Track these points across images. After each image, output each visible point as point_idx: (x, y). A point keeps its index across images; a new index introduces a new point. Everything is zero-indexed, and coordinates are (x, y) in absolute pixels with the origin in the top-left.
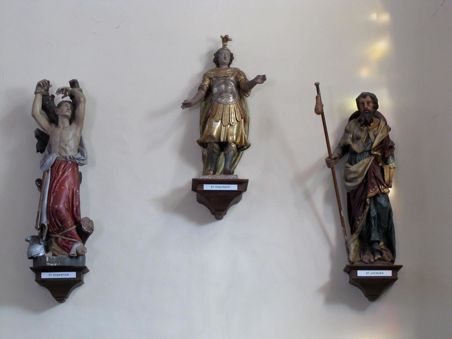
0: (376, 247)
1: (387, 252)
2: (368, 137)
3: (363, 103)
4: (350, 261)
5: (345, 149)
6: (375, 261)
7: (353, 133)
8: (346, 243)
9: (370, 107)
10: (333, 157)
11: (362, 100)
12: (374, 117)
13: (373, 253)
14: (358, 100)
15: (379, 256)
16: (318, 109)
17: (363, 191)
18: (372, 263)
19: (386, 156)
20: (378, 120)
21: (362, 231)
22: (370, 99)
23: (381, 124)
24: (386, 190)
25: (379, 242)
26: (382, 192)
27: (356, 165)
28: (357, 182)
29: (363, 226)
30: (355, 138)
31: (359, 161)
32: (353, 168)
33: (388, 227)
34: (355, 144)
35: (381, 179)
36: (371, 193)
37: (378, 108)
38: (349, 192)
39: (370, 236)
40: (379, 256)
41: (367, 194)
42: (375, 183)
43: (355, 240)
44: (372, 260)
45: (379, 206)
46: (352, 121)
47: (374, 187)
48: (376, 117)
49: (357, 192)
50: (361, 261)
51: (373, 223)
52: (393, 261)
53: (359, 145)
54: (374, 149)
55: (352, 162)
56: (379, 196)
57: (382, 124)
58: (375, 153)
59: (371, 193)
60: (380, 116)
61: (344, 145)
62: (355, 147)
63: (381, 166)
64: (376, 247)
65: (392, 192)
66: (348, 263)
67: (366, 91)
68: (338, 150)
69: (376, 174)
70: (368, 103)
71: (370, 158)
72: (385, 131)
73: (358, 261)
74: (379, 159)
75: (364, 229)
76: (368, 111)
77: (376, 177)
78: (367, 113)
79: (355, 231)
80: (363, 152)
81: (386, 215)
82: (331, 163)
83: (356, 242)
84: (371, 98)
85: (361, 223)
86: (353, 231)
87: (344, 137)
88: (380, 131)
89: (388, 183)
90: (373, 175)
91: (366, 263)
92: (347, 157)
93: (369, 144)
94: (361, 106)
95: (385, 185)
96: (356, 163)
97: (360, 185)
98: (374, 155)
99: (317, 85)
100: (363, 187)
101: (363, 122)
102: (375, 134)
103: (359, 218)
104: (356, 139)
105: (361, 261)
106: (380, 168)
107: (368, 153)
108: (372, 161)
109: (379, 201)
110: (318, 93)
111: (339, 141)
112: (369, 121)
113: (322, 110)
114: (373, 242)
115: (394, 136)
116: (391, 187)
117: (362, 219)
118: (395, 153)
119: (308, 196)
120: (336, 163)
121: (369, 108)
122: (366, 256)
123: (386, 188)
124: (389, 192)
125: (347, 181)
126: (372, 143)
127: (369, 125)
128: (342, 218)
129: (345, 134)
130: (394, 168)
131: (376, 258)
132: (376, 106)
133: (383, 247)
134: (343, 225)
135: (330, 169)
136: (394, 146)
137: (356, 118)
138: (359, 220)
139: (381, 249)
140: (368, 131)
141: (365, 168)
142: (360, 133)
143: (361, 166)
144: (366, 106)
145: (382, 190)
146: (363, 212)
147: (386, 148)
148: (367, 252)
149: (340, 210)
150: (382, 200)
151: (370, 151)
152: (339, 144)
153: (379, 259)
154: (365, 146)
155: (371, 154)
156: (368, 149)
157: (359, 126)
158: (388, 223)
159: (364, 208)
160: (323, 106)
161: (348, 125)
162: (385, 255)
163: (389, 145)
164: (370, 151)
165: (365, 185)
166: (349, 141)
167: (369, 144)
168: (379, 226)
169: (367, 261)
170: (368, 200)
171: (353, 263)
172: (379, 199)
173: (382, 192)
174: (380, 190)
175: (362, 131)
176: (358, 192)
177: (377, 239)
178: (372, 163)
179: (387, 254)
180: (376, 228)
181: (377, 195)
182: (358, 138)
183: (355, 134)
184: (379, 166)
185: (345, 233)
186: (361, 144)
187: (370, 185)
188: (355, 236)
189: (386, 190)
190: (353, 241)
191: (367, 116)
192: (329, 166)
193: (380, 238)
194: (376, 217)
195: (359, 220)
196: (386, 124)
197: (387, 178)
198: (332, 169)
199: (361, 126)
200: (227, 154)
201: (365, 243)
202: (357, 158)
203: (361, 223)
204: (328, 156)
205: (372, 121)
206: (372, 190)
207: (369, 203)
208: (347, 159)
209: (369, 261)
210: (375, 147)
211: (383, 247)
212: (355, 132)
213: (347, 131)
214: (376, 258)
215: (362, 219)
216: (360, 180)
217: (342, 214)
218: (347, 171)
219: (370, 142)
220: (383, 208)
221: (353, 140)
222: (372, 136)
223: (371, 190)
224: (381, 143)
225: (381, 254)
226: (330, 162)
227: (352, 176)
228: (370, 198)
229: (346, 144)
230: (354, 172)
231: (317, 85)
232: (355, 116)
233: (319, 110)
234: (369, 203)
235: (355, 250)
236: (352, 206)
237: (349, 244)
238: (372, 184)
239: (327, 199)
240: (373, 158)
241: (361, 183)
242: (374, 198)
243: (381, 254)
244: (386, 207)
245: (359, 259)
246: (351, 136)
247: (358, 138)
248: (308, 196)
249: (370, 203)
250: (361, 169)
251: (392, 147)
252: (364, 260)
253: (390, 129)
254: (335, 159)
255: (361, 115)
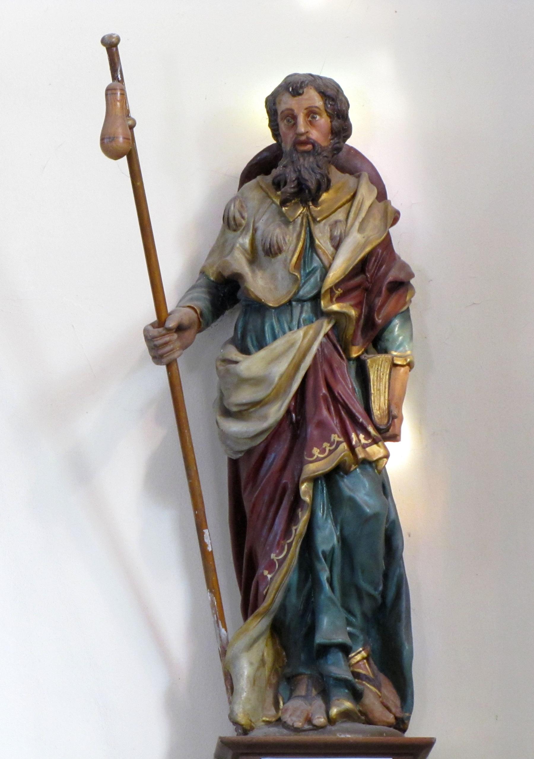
0: (337, 667)
1: (379, 688)
2: (311, 245)
3: (292, 117)
4: (235, 723)
5: (224, 293)
6: (331, 721)
7: (255, 230)
8: (223, 653)
9: (318, 132)
10: (171, 323)
11: (288, 102)
12: (333, 169)
13: (325, 689)
14: (272, 104)
15: (348, 705)
16: (113, 139)
17: (290, 451)
18: (316, 728)
19: (379, 321)
20: (351, 180)
21: (283, 607)
22: (318, 102)
23: (359, 197)
24: (375, 451)
25: (346, 650)
26: (361, 456)
27: (262, 353)
28: (265, 418)
29: (288, 590)
30: (260, 248)
31: (275, 338)
32: (251, 365)
33: (384, 595)
34: (259, 274)
35: (358, 409)
36: (318, 463)
37: (348, 136)
38: (235, 457)
39: (312, 630)
40: (348, 705)
41: (302, 463)
42: (334, 423)
43: (256, 640)
44: (320, 720)
45: (347, 512)
46: (253, 182)
47: (328, 440)
48: (343, 169)
49: (263, 456)
50: (279, 722)
51: (324, 576)
52: (401, 724)
53: (273, 277)
54: (331, 290)
55: (247, 341)
56: (347, 472)
57: (366, 195)
58: (335, 307)
59: (318, 463)
60: (355, 166)
61: (220, 275)
62: (262, 285)
63: (358, 358)
64: (337, 667)
65: (401, 458)
66: (230, 732)
67: (303, 69)
68: (196, 294)
69: (339, 389)
70: (311, 113)
71: (315, 325)
72: (375, 222)
73: (268, 723)
74: (350, 331)
75: (293, 599)
76: (309, 147)
77: (338, 401)
78: (305, 154)
79: (256, 607)
80: (290, 302)
81: (376, 546)
82: (166, 344)
83: (264, 649)
84: (323, 95)
85: (279, 576)
86: (249, 606)
87: (222, 247)
88: (357, 225)
89: (382, 423)
90: (324, 391)
91: (297, 730)
92: (228, 324)
93: (314, 271)
94: (283, 126)
95: (371, 429)
96: (261, 345)
97: (275, 433)
98: (329, 315)
99: (111, 46)
100: (287, 436)
101: (290, 188)
102: (337, 233)
103: (273, 556)
104: (263, 253)
105: (279, 722)
106: (353, 366)
107: (308, 306)
108: (321, 337)
109: (347, 492)
110: (114, 77)
111: (203, 262)
112: (312, 184)
113: (131, 140)
114: (325, 649)
115: (409, 243)
116: (395, 438)
117: (281, 562)
118: (416, 304)
119: (81, 471)
120: (185, 347)
121: (315, 135)
122: (295, 704)
123: (375, 442)
124: (387, 456)
125: (227, 413)
126: (325, 271)
127: (315, 200)
128: (207, 557)
129: (223, 233)
130: (410, 365)
131: (334, 711)
132: (341, 128)
133: (365, 669)
134: (212, 584)
135: (164, 368)
136: (412, 281)
137: (267, 172)
138: (271, 566)
139: (356, 675)
140: (310, 221)
141: (297, 367)
142: (278, 231)
143: (285, 355)
144: (302, 127)
145: (358, 450)
146: (287, 533)
147: (379, 287)
148: (302, 690)
149: (201, 525)
150: (359, 490)
151: (316, 299)
152: (203, 273)
153: (346, 715)
154: (296, 280)
155: (319, 313)
156: (307, 290)
157: (278, 202)
158: (386, 576)
159: (292, 519)
160: (131, 128)
161: (234, 199)
162: (371, 699)
163: (390, 278)
164: (316, 299)
165: (295, 428)
166: (239, 262)
167: (314, 271)
168: (350, 590)
169: (298, 724)
170: (304, 487)
171: (245, 732)
172: (346, 485)
173: (361, 456)
174: (352, 448)
175: (287, 222)
176: (271, 457)
177: (341, 638)
178: (321, 344)
179: (378, 697)
180: (337, 597)
181: (339, 470)
182: (272, 251)
183: (259, 233)
184: (349, 359)
185: (220, 618)
186: (281, 273)
187: (312, 431)
188: (259, 625)
189: (375, 451)
190: (250, 646)
191: (306, 164)
192: (157, 358)
193: (350, 634)
194: (338, 553)
195: (271, 566)
196: (382, 195)
197: (379, 404)
198: (169, 366)
199: (283, 203)
200: (271, 204)
201: (297, 654)
202: (267, 328)
203: (279, 576)
204: (153, 317)
205: (324, 184)
206: (323, 451)
207: (307, 499)
208: (231, 334)
209: (309, 721)
210: (337, 285)
211: (365, 669)
212: (261, 225)
213: (231, 224)
214: (334, 711)
215: (281, 562)
216: (275, 412)
217: (207, 540)
218: (228, 377)
219: (316, 263)
220: (365, 520)
221: (253, 259)
222: (323, 242)
223: (316, 451)
224: (361, 267)
225: (357, 695)
226: (164, 340)
227: (245, 395)
228: (315, 480)
229: (226, 274)
230: (255, 381)
231: (111, 46)
232: (261, 167)
233: (119, 142)
234: (307, 499)
235: (254, 681)
236: (247, 510)
237: (236, 658)
238: (321, 424)
239: (154, 482)
240: (326, 327)
241: (280, 423)
242: (331, 479)
243: (357, 695)
244: (376, 516)
245: (271, 714)
246: (246, 241)
247: (272, 251)
248: (81, 471)
249: (314, 499)
250: (280, 368)
251: (401, 286)
252: (288, 718)
253: (396, 217)
254: (180, 329)
255: (283, 162)
